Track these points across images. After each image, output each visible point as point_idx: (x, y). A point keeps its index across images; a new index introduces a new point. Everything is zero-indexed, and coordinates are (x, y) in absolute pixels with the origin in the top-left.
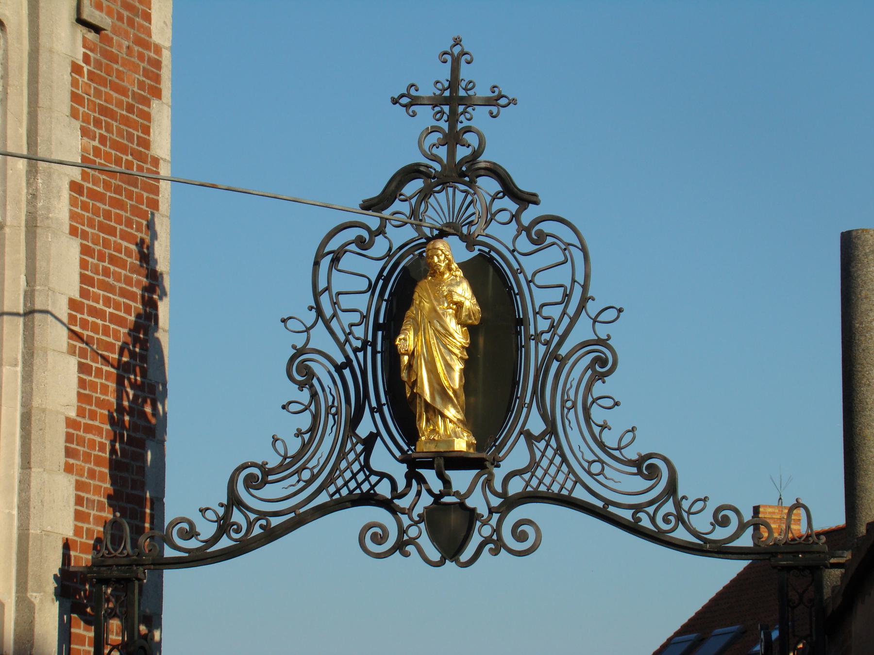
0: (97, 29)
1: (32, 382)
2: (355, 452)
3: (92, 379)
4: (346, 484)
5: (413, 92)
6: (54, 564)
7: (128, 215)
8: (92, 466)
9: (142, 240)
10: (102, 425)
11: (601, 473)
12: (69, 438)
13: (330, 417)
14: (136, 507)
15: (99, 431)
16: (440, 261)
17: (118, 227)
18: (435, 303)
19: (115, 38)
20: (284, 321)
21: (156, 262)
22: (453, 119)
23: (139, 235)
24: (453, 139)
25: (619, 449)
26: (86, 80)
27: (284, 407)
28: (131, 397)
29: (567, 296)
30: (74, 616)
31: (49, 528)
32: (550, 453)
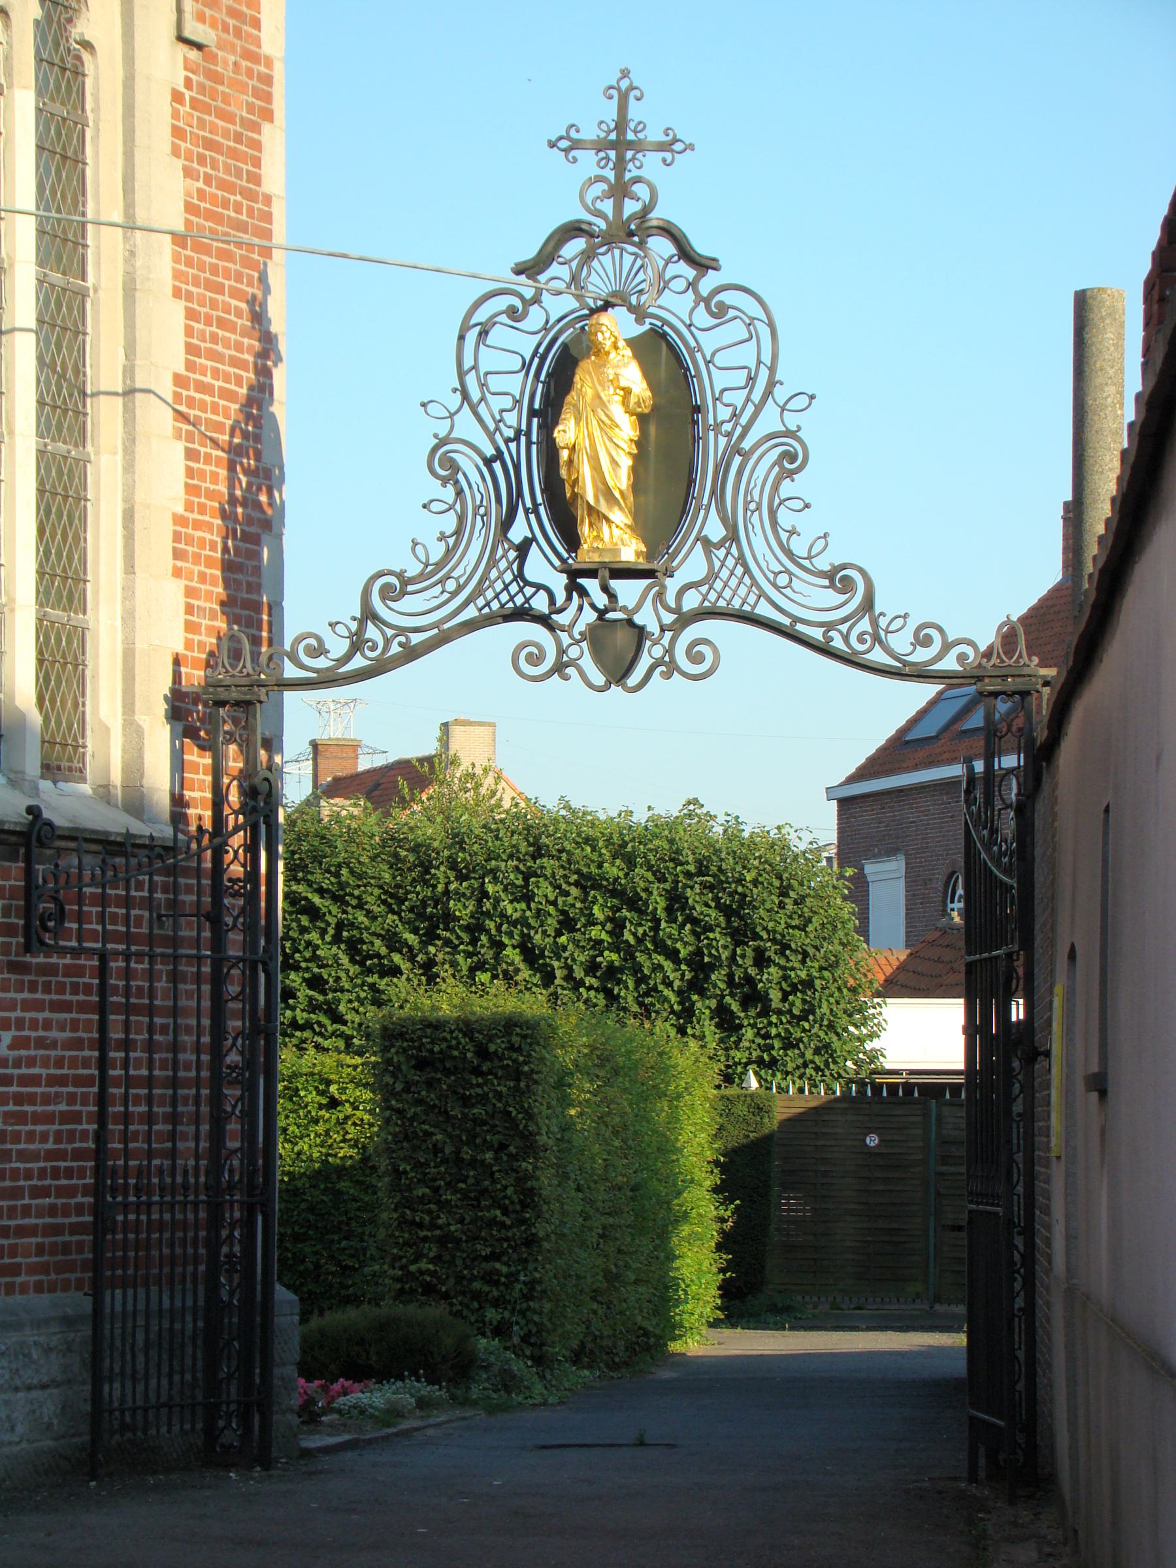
0: (199, 47)
1: (134, 473)
2: (507, 560)
3: (201, 466)
4: (497, 596)
5: (573, 134)
6: (165, 685)
7: (238, 267)
8: (202, 568)
9: (254, 297)
10: (212, 520)
11: (789, 586)
12: (177, 537)
13: (479, 518)
14: (252, 614)
15: (209, 527)
16: (604, 339)
17: (227, 283)
18: (599, 389)
19: (220, 53)
20: (424, 405)
21: (269, 321)
22: (620, 166)
23: (250, 290)
24: (620, 190)
25: (809, 558)
26: (188, 109)
27: (425, 506)
28: (244, 485)
29: (751, 380)
30: (187, 740)
31: (157, 642)
32: (730, 562)
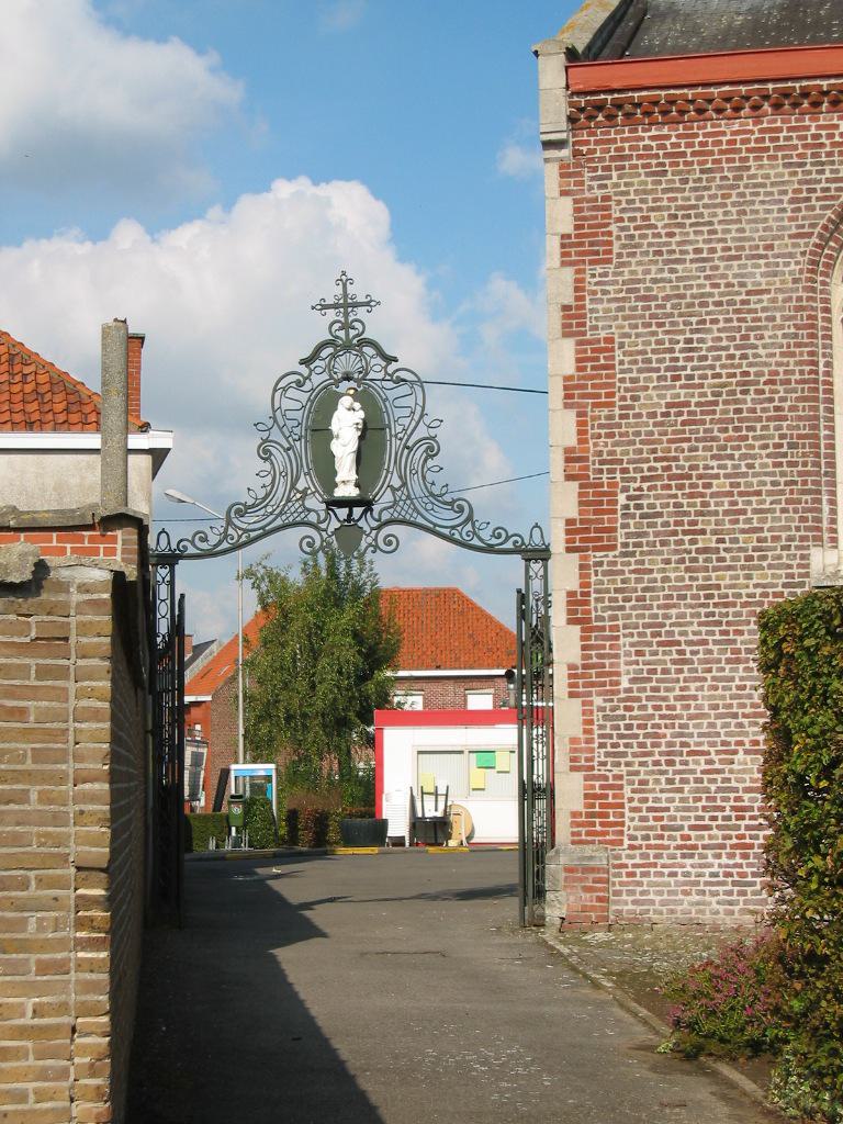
22: (346, 315)
